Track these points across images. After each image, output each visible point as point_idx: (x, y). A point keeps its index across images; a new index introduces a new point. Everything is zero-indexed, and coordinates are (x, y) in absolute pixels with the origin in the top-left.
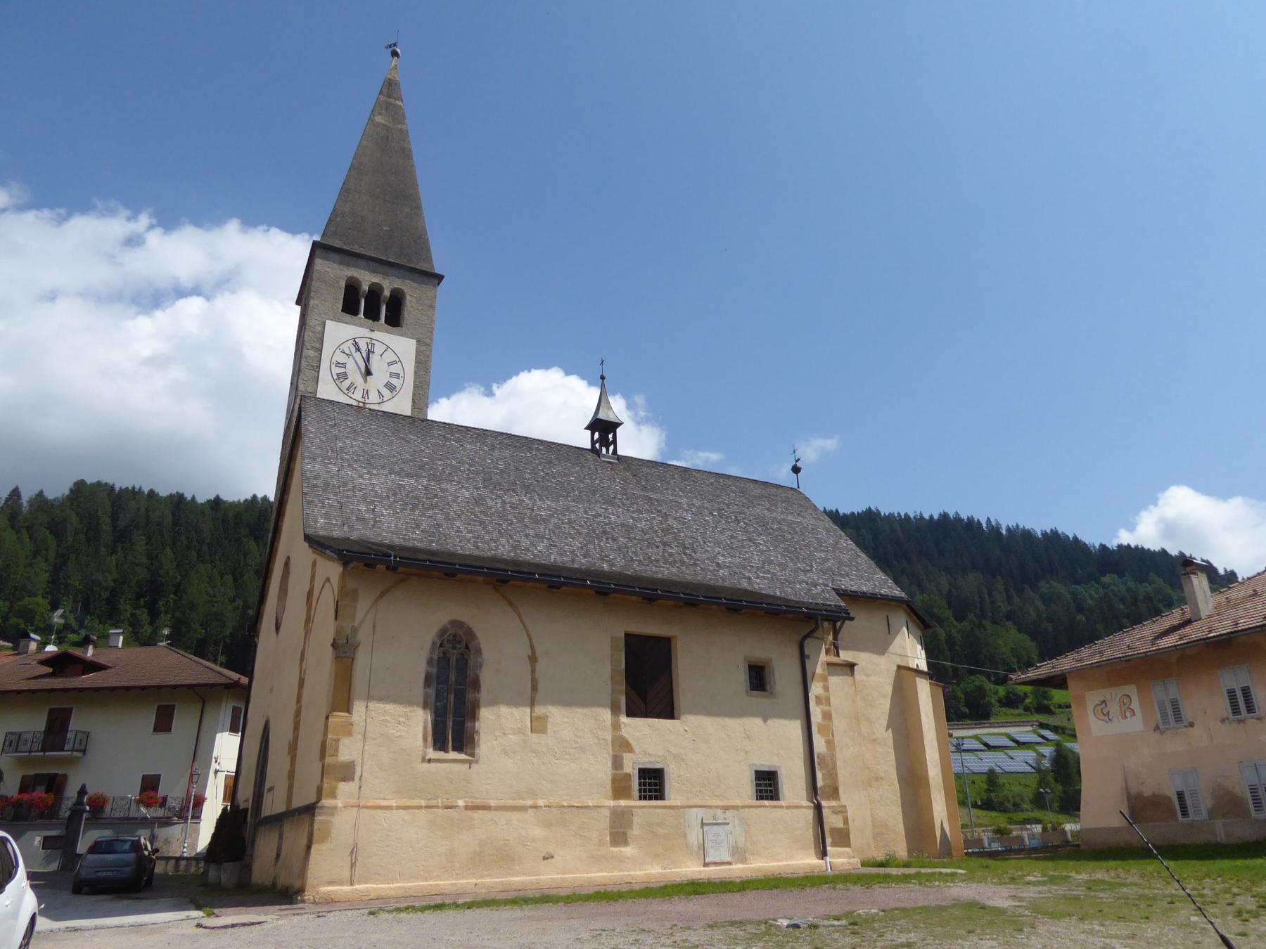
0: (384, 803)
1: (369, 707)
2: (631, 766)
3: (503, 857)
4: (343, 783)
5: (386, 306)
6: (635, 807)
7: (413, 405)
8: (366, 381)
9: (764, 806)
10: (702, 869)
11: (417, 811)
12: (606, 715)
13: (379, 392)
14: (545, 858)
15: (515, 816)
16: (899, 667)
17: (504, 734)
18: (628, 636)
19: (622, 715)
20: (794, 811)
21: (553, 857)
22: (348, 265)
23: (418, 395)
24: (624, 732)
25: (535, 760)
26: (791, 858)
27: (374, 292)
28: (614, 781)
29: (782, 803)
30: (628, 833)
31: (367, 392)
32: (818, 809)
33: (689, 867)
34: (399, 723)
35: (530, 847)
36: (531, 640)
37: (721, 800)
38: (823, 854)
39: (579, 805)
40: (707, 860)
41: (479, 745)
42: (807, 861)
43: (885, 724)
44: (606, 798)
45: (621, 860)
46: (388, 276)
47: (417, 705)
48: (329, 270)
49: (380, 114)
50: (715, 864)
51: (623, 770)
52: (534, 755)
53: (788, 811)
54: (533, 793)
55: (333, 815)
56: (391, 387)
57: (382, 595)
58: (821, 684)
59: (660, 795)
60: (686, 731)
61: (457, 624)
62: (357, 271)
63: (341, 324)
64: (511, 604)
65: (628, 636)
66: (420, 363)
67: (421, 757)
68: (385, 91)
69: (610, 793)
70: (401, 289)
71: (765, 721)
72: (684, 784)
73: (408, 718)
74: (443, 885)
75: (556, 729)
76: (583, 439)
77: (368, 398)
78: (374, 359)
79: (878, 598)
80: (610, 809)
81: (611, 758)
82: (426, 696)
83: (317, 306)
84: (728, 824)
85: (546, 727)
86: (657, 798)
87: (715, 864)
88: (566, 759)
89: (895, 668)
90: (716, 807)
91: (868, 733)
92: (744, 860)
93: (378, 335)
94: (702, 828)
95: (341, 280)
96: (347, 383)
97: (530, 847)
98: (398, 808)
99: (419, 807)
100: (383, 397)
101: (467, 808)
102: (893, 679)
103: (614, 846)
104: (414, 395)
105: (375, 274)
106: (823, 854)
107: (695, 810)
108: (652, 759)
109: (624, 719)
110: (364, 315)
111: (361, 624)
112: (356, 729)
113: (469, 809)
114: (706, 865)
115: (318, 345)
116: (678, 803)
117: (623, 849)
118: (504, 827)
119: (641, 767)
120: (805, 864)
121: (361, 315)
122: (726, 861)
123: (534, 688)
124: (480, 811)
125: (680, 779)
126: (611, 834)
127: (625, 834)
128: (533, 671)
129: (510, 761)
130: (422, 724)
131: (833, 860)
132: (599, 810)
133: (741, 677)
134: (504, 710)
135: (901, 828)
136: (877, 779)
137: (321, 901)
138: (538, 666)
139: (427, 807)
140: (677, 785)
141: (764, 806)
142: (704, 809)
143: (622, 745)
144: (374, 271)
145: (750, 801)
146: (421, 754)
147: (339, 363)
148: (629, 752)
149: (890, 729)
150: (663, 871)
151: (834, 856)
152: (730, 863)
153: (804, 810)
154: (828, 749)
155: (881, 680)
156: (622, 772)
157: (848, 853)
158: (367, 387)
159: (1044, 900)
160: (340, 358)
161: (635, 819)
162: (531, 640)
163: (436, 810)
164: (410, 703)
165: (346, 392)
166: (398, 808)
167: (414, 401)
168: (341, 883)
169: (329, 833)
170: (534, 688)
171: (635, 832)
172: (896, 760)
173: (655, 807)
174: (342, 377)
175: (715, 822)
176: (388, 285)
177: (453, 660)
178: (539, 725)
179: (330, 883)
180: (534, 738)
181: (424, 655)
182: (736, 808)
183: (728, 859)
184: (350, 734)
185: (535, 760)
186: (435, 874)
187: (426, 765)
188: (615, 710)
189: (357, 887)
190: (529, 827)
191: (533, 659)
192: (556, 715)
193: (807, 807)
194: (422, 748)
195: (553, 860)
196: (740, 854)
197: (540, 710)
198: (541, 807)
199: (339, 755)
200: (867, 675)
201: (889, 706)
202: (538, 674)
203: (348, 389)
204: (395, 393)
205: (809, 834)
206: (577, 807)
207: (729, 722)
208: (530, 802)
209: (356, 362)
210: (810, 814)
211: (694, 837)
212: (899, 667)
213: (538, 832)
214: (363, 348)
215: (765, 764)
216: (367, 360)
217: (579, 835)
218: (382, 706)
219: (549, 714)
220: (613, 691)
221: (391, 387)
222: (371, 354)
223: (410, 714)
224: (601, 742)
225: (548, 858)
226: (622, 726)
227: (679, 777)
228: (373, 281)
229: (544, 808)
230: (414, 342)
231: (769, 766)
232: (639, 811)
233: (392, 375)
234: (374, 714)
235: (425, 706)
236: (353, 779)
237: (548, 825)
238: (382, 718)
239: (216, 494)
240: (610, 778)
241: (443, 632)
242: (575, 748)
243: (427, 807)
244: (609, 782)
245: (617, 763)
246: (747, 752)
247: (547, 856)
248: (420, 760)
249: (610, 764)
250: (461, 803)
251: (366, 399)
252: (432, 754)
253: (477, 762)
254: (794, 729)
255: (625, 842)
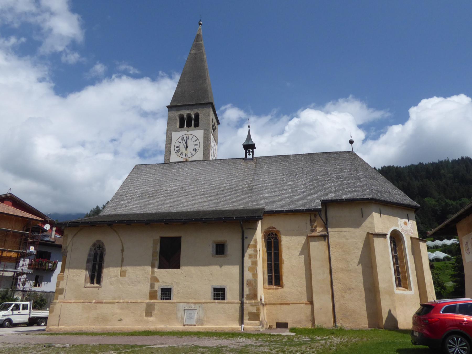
0: (70, 301)
1: (69, 271)
2: (157, 287)
3: (104, 319)
4: (60, 295)
5: (194, 121)
6: (156, 303)
7: (203, 154)
8: (186, 150)
9: (215, 303)
10: (182, 327)
11: (79, 304)
12: (149, 268)
13: (191, 153)
14: (119, 320)
15: (110, 305)
16: (368, 233)
17: (111, 277)
18: (162, 238)
19: (156, 268)
20: (230, 305)
21: (122, 320)
22: (179, 110)
23: (205, 150)
24: (156, 275)
25: (121, 286)
26: (226, 324)
27: (189, 116)
28: (150, 293)
29: (225, 301)
30: (153, 312)
31: (187, 154)
32: (242, 303)
33: (176, 326)
34: (78, 275)
35: (114, 316)
36: (122, 244)
37: (196, 300)
38: (241, 322)
39: (135, 302)
40: (185, 323)
41: (102, 281)
42: (235, 326)
43: (357, 262)
44: (147, 299)
45: (148, 322)
46: (192, 109)
47: (84, 269)
48: (172, 114)
49: (193, 50)
50: (188, 325)
51: (154, 289)
52: (121, 284)
53: (226, 305)
54: (119, 298)
55: (55, 305)
56: (195, 150)
57: (75, 235)
58: (253, 249)
59: (223, 298)
60: (182, 273)
61: (98, 241)
62: (182, 111)
63: (177, 132)
64: (116, 232)
65: (162, 238)
66: (205, 138)
67: (83, 286)
68: (196, 40)
69: (148, 297)
70: (198, 113)
71: (221, 267)
72: (179, 294)
73: (80, 273)
74: (84, 328)
75: (129, 275)
76: (241, 153)
77: (187, 156)
78: (189, 142)
79: (344, 201)
80: (146, 303)
81: (150, 285)
82: (87, 266)
83: (169, 128)
84: (196, 310)
85: (126, 274)
86: (222, 299)
87: (188, 325)
88: (132, 285)
89: (366, 234)
90: (192, 303)
91: (345, 267)
92: (202, 324)
93: (190, 132)
94: (184, 311)
95: (176, 117)
96: (180, 152)
97: (114, 316)
98: (74, 303)
99: (80, 303)
100: (192, 154)
101: (95, 303)
102: (364, 239)
103: (146, 317)
104: (204, 150)
105: (188, 110)
106: (241, 322)
107: (182, 304)
108: (167, 285)
109: (156, 270)
110: (186, 127)
111: (69, 244)
112: (65, 278)
113: (96, 303)
114: (184, 325)
115: (170, 142)
116: (175, 301)
117: (149, 318)
118: (105, 309)
119: (162, 287)
120: (230, 327)
121: (185, 127)
122: (193, 324)
123: (123, 261)
124: (99, 304)
125: (179, 292)
126: (146, 312)
127: (151, 313)
128: (122, 255)
129: (112, 287)
130: (85, 275)
131: (245, 326)
132: (142, 304)
133: (211, 249)
134: (111, 269)
135: (365, 313)
136: (350, 289)
137: (49, 331)
138: (124, 253)
139: (83, 302)
140: (177, 294)
141: (215, 303)
142: (186, 304)
143: (155, 280)
144: (188, 109)
145: (210, 300)
146: (83, 285)
147: (177, 146)
148: (157, 282)
149: (360, 265)
150: (164, 327)
151: (248, 324)
152: (195, 325)
153: (235, 304)
154: (253, 277)
155: (356, 240)
156: (154, 290)
157: (256, 324)
158: (187, 152)
159: (163, 342)
160: (177, 144)
161: (156, 307)
162: (122, 244)
163: (85, 303)
164: (81, 268)
165: (180, 156)
166: (74, 303)
167: (204, 153)
168: (55, 325)
169: (54, 310)
170: (123, 261)
171: (155, 312)
172: (363, 279)
173: (165, 303)
174: (178, 151)
175: (190, 309)
176: (193, 113)
177: (99, 254)
178: (123, 274)
179: (53, 325)
180: (121, 278)
181: (87, 252)
182: (201, 303)
183: (195, 323)
184: (63, 280)
185: (121, 286)
186: (83, 324)
187: (85, 289)
188: (153, 266)
189: (60, 327)
190: (116, 309)
191: (123, 251)
192: (129, 270)
193: (237, 303)
194: (84, 283)
195: (122, 321)
196: (200, 321)
197: (124, 268)
198: (120, 302)
199: (60, 286)
200: (347, 239)
201: (360, 253)
202: (124, 256)
203: (180, 155)
204: (197, 151)
205: (237, 314)
206: (133, 302)
207: (202, 268)
208: (117, 301)
209: (183, 144)
210: (238, 306)
211: (180, 314)
212: (368, 233)
213: (118, 311)
214: (185, 138)
215: (219, 285)
216: (186, 143)
217: (133, 312)
218: (73, 270)
219: (127, 270)
220: (153, 259)
221: (195, 150)
222: (188, 140)
223: (81, 272)
224: (146, 279)
225: (120, 320)
226: (155, 272)
227: (177, 291)
228: (188, 113)
229: (121, 303)
230: (203, 131)
231: (220, 286)
232: (158, 304)
233: (196, 145)
234: (70, 273)
235: (86, 269)
236: (63, 294)
237: (122, 309)
238: (72, 274)
239: (97, 205)
240: (149, 292)
241: (94, 245)
242: (136, 281)
243: (83, 302)
244: (148, 294)
245: (152, 286)
246: (210, 281)
247: (120, 319)
248: (83, 287)
249: (149, 287)
250: (94, 301)
251: (187, 157)
252: (89, 285)
253: (101, 287)
254: (236, 270)
255: (151, 316)
